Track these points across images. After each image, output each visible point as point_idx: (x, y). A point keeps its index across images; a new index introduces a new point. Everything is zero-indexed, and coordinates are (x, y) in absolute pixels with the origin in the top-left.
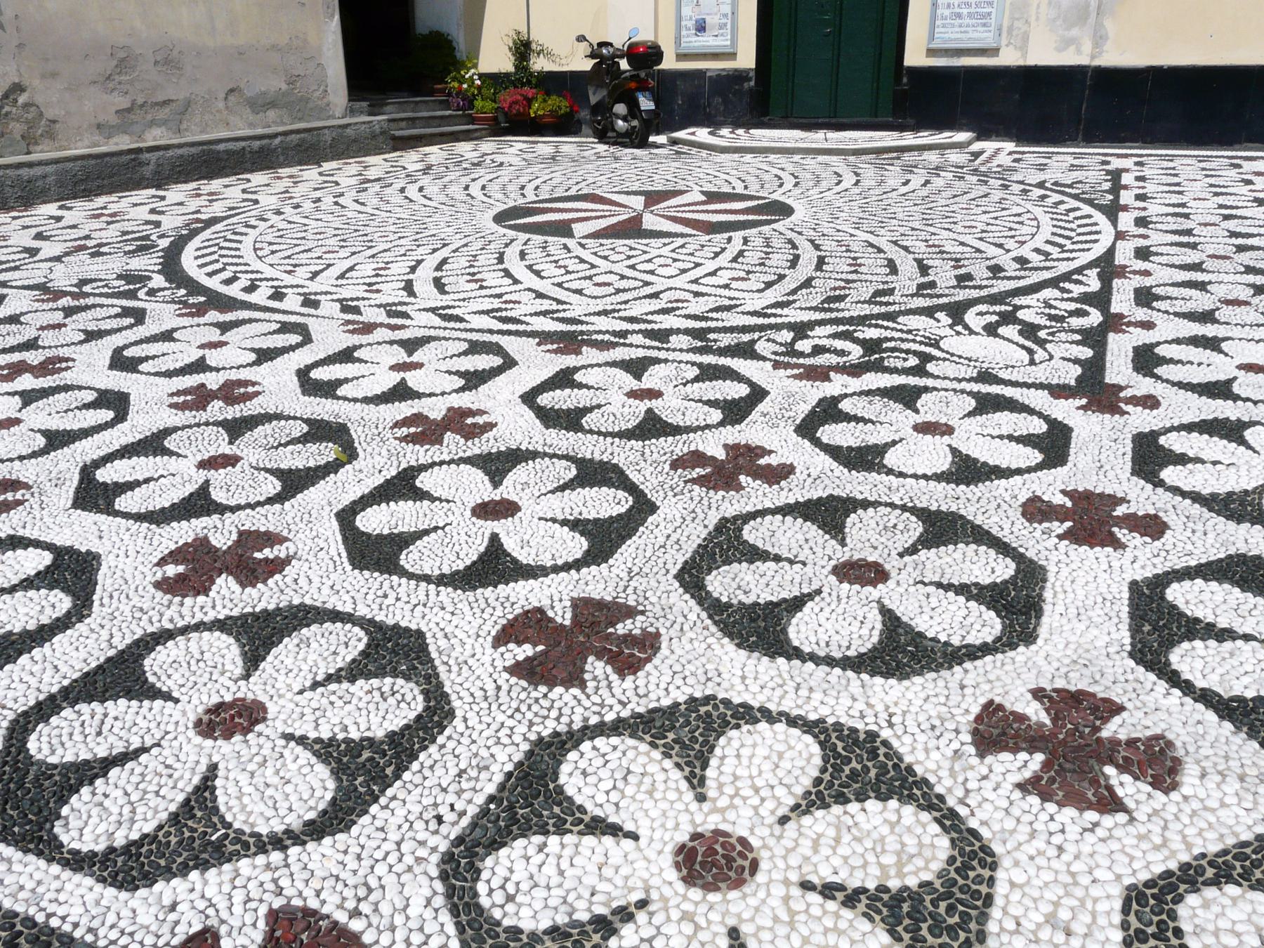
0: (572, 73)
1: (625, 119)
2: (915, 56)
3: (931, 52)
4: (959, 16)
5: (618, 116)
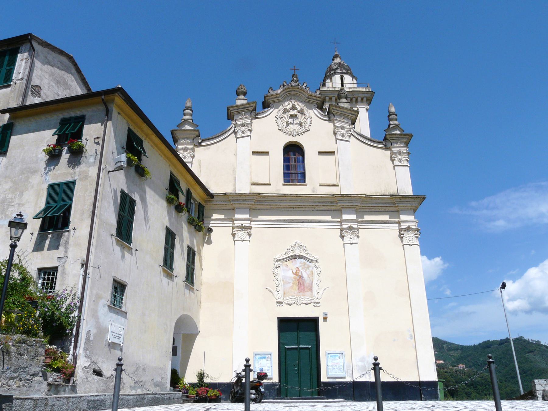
0: (219, 383)
1: (254, 394)
2: (324, 379)
3: (328, 378)
4: (334, 369)
5: (252, 394)
